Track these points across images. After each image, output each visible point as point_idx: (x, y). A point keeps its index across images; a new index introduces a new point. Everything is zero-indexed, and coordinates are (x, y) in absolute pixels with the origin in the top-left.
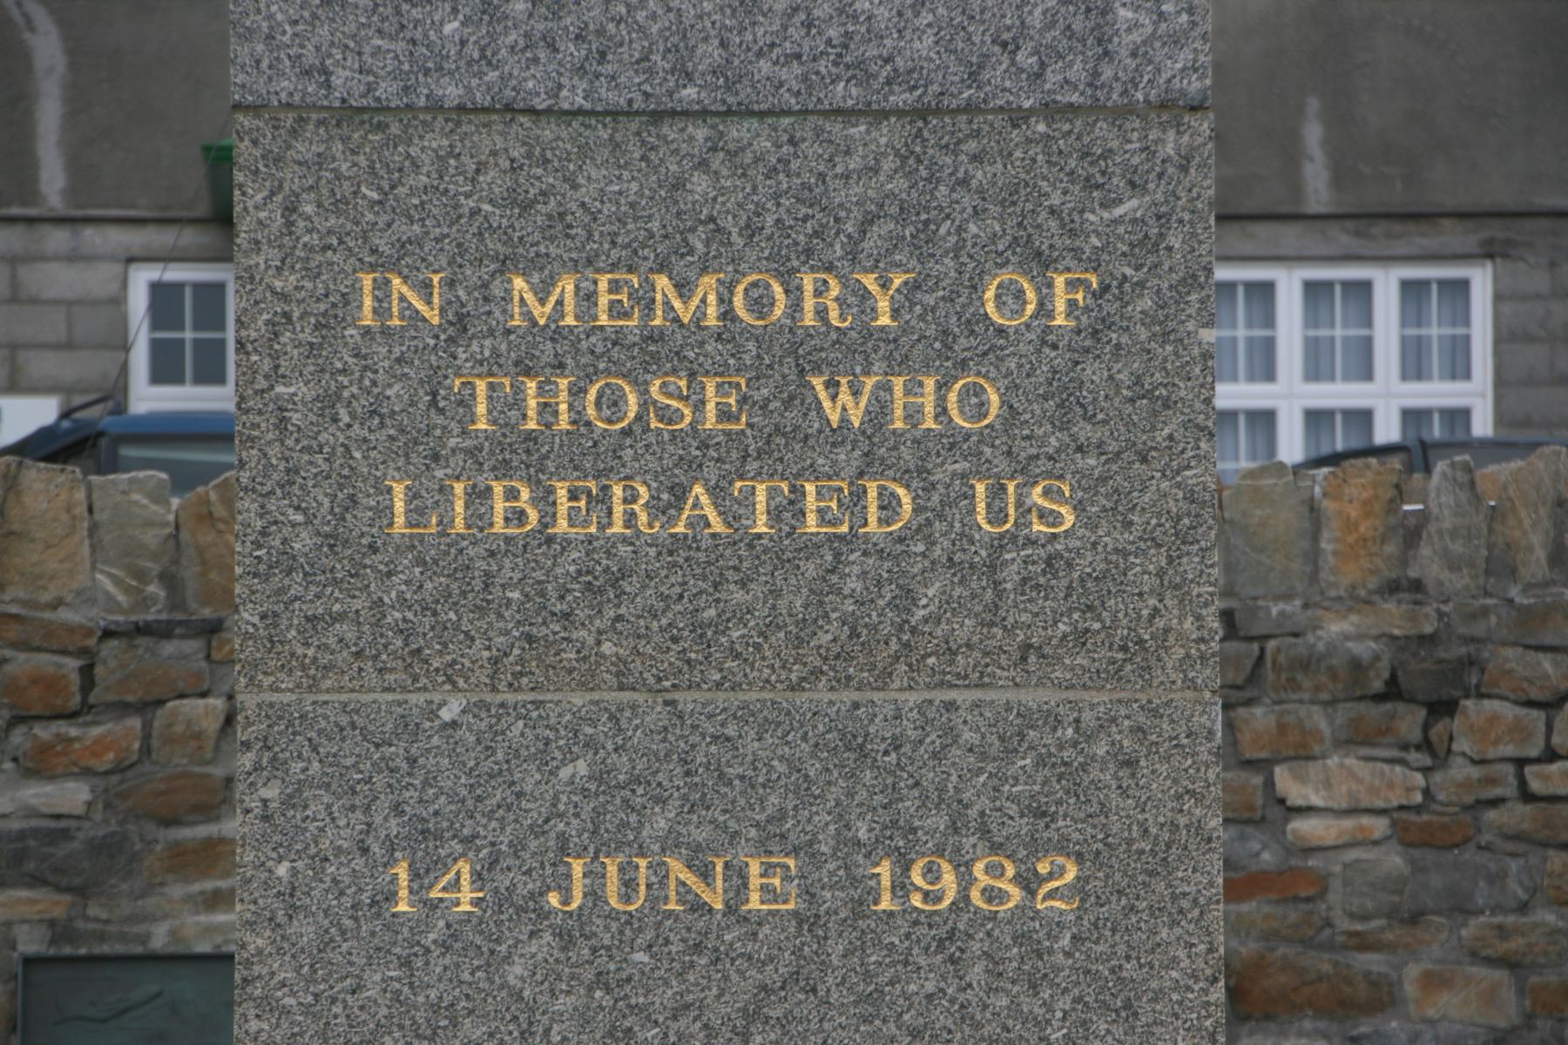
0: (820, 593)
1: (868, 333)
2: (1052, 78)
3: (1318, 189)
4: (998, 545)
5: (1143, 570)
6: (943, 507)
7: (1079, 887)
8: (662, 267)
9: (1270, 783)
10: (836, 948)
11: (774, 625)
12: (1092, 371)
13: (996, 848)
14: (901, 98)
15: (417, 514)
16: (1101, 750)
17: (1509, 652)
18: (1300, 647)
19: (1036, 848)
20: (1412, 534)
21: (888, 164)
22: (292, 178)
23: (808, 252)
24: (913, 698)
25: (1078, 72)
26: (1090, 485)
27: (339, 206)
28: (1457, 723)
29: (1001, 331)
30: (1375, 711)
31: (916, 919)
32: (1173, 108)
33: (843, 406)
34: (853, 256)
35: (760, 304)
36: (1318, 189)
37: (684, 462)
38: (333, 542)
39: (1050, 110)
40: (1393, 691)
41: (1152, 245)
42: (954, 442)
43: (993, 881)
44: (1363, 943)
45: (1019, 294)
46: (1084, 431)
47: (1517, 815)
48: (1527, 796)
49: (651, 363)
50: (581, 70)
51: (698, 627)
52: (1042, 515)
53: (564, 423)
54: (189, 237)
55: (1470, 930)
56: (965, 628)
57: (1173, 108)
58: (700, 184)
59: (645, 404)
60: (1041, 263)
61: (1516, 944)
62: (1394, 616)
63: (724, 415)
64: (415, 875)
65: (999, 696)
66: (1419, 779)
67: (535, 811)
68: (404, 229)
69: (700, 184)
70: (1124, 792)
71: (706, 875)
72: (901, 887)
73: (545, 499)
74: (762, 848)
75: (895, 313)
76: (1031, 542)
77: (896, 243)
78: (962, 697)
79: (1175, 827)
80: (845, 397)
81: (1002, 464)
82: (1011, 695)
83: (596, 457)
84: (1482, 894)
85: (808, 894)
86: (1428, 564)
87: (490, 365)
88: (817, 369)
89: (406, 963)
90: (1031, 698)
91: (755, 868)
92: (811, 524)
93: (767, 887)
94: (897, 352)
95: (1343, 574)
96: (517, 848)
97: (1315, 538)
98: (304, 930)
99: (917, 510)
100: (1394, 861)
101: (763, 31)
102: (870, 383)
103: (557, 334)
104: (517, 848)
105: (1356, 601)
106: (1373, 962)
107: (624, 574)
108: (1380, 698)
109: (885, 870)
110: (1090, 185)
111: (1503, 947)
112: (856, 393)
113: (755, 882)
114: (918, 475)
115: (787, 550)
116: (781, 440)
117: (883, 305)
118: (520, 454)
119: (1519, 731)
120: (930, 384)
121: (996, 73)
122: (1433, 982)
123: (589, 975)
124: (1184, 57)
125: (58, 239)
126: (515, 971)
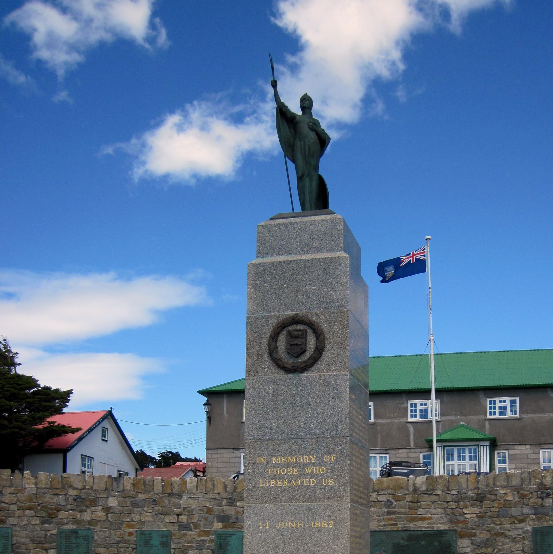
1: (311, 463)
2: (332, 434)
4: (325, 486)
5: (341, 489)
6: (319, 482)
7: (334, 524)
10: (307, 532)
11: (301, 495)
12: (336, 466)
14: (315, 436)
15: (263, 484)
19: (329, 520)
20: (478, 482)
22: (250, 448)
25: (334, 433)
26: (335, 479)
31: (316, 528)
32: (344, 437)
33: (308, 471)
34: (310, 454)
35: (300, 460)
37: (292, 477)
38: (254, 487)
39: (331, 437)
40: (476, 500)
42: (321, 475)
44: (473, 529)
46: (335, 473)
51: (293, 496)
54: (426, 450)
56: (322, 496)
57: (344, 437)
58: (293, 446)
60: (330, 454)
62: (476, 491)
63: (296, 472)
67: (275, 517)
69: (293, 446)
71: (293, 524)
72: (314, 525)
73: (276, 482)
74: (299, 520)
78: (321, 503)
83: (282, 477)
84: (486, 523)
85: (304, 526)
90: (328, 503)
92: (305, 484)
93: (300, 525)
94: (314, 465)
95: (471, 486)
98: (251, 530)
100: (476, 519)
101: (301, 429)
104: (273, 520)
105: (472, 490)
106: (474, 531)
110: (336, 445)
115: (302, 487)
116: (302, 475)
121: (326, 434)
122: (481, 533)
124: (346, 431)
125: (413, 450)
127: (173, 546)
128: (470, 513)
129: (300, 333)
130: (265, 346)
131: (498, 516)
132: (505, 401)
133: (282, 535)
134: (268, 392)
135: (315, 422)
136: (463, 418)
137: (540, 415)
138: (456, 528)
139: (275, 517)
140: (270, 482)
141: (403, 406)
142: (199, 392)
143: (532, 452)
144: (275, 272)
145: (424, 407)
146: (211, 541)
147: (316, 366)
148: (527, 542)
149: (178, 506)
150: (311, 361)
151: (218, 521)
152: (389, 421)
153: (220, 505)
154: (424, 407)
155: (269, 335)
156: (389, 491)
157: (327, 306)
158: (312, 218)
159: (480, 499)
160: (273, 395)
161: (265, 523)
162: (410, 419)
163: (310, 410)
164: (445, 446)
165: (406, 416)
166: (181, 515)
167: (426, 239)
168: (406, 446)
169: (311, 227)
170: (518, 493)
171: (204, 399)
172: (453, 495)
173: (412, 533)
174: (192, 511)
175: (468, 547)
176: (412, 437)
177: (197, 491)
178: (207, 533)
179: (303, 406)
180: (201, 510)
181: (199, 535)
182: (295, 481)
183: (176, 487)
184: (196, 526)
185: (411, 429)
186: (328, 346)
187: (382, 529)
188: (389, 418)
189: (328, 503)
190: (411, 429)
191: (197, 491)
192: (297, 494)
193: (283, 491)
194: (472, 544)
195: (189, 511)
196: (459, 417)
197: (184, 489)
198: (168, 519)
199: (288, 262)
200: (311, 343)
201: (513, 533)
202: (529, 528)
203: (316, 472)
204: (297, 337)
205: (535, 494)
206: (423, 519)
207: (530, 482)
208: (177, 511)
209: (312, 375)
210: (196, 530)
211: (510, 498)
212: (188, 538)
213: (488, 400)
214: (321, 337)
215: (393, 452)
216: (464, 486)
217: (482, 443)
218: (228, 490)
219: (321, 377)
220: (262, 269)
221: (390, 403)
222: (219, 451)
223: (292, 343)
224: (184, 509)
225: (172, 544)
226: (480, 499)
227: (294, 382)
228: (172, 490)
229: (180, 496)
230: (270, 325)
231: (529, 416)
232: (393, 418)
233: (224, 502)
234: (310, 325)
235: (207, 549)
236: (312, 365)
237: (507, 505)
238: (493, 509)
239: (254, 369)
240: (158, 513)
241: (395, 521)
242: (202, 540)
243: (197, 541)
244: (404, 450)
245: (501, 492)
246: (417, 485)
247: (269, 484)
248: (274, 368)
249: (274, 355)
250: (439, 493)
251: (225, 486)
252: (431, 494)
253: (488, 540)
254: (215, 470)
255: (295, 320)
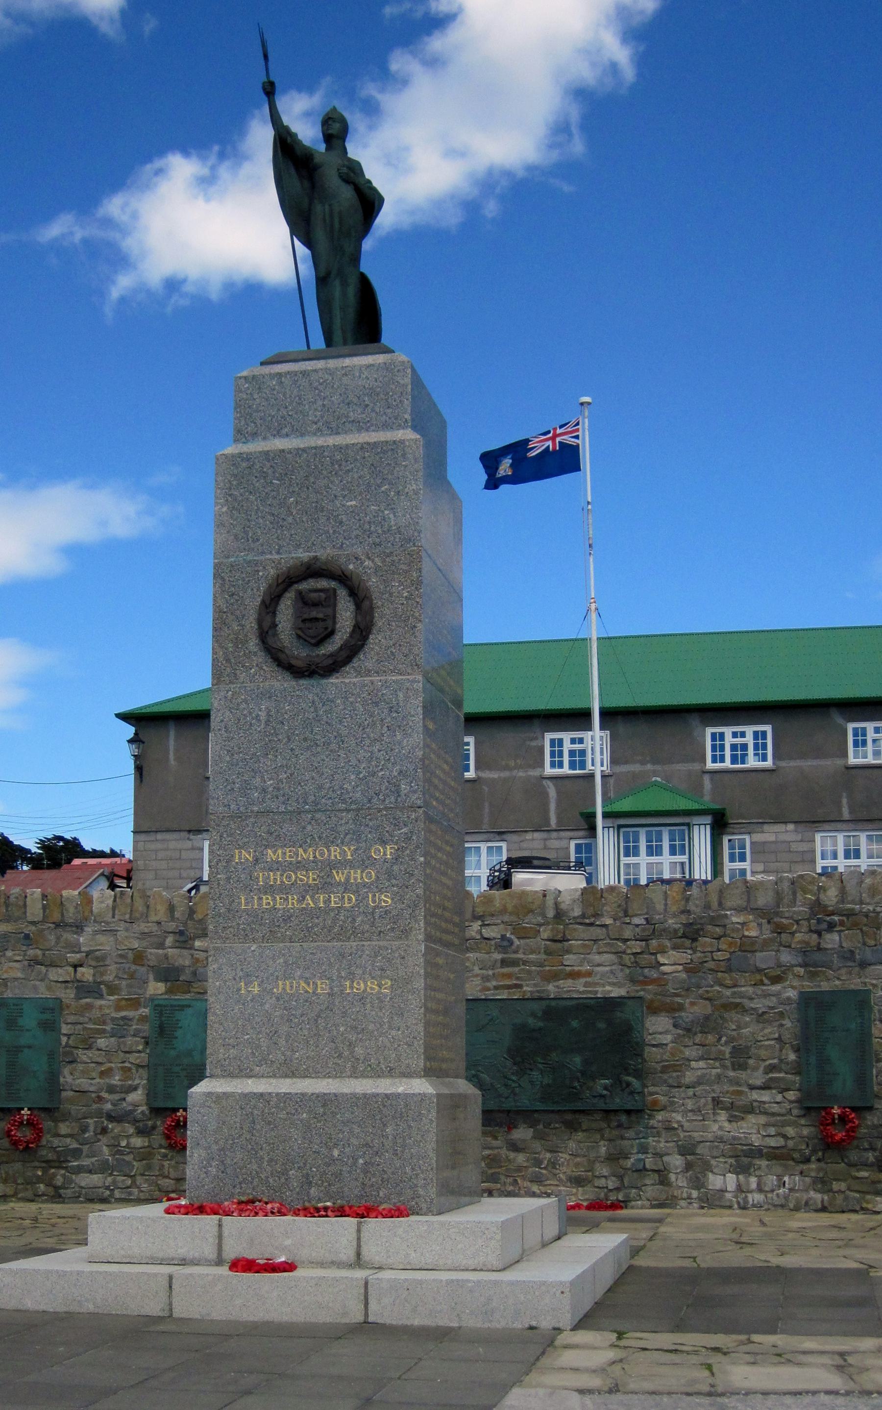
0: (335, 920)
2: (387, 801)
3: (846, 815)
4: (375, 908)
8: (301, 846)
9: (656, 958)
12: (395, 868)
13: (373, 978)
15: (247, 904)
16: (397, 955)
17: (710, 927)
18: (662, 926)
19: (382, 977)
20: (687, 899)
21: (351, 822)
23: (333, 842)
24: (355, 944)
25: (393, 799)
27: (231, 835)
28: (698, 944)
29: (375, 859)
30: (679, 940)
32: (414, 807)
33: (339, 877)
34: (342, 843)
35: (322, 855)
36: (846, 815)
37: (307, 890)
38: (229, 910)
39: (386, 808)
41: (410, 839)
42: (365, 885)
43: (372, 986)
45: (379, 851)
46: (394, 881)
47: (711, 965)
48: (714, 960)
49: (298, 868)
50: (284, 803)
51: (308, 928)
52: (384, 901)
53: (279, 882)
55: (701, 991)
56: (367, 927)
57: (414, 807)
58: (309, 828)
59: (297, 877)
60: (384, 843)
61: (710, 995)
63: (314, 880)
64: (246, 985)
65: (374, 943)
66: (690, 957)
67: (271, 970)
68: (246, 840)
69: (309, 828)
70: (402, 965)
71: (309, 985)
72: (352, 987)
73: (274, 899)
74: (321, 978)
75: (352, 856)
76: (382, 907)
77: (352, 839)
79: (412, 972)
80: (340, 875)
81: (375, 890)
82: (377, 943)
83: (284, 890)
85: (331, 988)
86: (691, 907)
87: (263, 870)
88: (334, 868)
89: (244, 1004)
90: (381, 943)
91: (319, 983)
92: (333, 904)
94: (351, 864)
95: (674, 909)
96: (268, 978)
97: (666, 900)
99: (356, 900)
100: (684, 976)
102: (345, 871)
103: (278, 862)
104: (268, 978)
105: (674, 916)
107: (292, 916)
108: (681, 937)
109: (348, 983)
110: (395, 825)
111: (706, 996)
112: (343, 874)
113: (319, 986)
114: (356, 892)
115: (327, 910)
116: (326, 885)
117: (349, 854)
118: (269, 889)
119: (711, 945)
120: (359, 871)
121: (374, 801)
122: (692, 1004)
123: (282, 1007)
124: (416, 796)
125: (554, 834)
126: (267, 1006)
127: (65, 1029)
128: (672, 962)
129: (323, 595)
130: (251, 623)
131: (729, 970)
132: (743, 734)
133: (285, 1008)
134: (258, 715)
135: (353, 777)
136: (658, 767)
137: (815, 763)
138: (642, 993)
139: (271, 970)
140: (260, 899)
141: (534, 744)
142: (118, 716)
143: (799, 837)
144: (270, 472)
145: (577, 746)
146: (143, 1019)
147: (355, 663)
148: (787, 1023)
149: (75, 948)
150: (344, 654)
151: (158, 979)
152: (505, 774)
153: (161, 946)
154: (577, 746)
155: (259, 600)
156: (506, 918)
157: (378, 540)
158: (348, 362)
159: (691, 934)
160: (267, 723)
161: (251, 982)
162: (549, 771)
163: (341, 753)
164: (620, 827)
165: (542, 765)
166: (81, 966)
167: (582, 404)
168: (542, 827)
169: (345, 380)
170: (769, 922)
171: (129, 731)
172: (637, 926)
173: (553, 1003)
174: (103, 958)
175: (666, 1032)
176: (553, 806)
177: (113, 917)
178: (135, 1003)
179: (329, 744)
180: (121, 956)
181: (118, 1008)
182: (312, 897)
183: (72, 910)
184: (113, 989)
185: (552, 792)
186: (379, 623)
187: (490, 994)
188: (507, 768)
189: (381, 943)
190: (552, 792)
191: (113, 917)
192: (317, 925)
193: (287, 918)
194: (675, 1026)
195: (97, 959)
196: (649, 767)
197: (86, 914)
198: (56, 974)
199: (299, 452)
200: (345, 615)
201: (759, 1005)
202: (792, 994)
203: (355, 879)
204: (316, 604)
205: (805, 923)
206: (574, 975)
207: (795, 899)
208: (73, 957)
209: (347, 681)
210: (112, 998)
211: (753, 933)
212: (96, 1013)
213: (709, 731)
214: (366, 603)
215: (514, 838)
216: (660, 907)
217: (696, 820)
218: (177, 915)
219: (364, 686)
220: (244, 465)
221: (508, 737)
222: (159, 836)
223: (306, 616)
224: (88, 954)
225: (64, 1026)
226: (691, 934)
227: (310, 696)
228: (62, 915)
229: (79, 928)
230: (263, 580)
231: (792, 763)
232: (515, 768)
233: (169, 941)
234: (343, 578)
235: (134, 1035)
236: (348, 660)
237: (748, 947)
238: (719, 955)
239: (228, 669)
240: (35, 962)
241: (518, 978)
242: (124, 1018)
243: (113, 1019)
244: (537, 835)
245: (735, 919)
246: (563, 906)
247: (260, 905)
248: (269, 667)
249: (270, 641)
250: (609, 921)
251: (171, 908)
252: (591, 924)
253: (707, 1018)
254: (151, 875)
255: (312, 570)
